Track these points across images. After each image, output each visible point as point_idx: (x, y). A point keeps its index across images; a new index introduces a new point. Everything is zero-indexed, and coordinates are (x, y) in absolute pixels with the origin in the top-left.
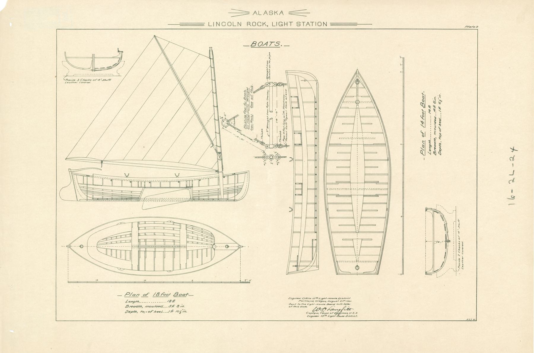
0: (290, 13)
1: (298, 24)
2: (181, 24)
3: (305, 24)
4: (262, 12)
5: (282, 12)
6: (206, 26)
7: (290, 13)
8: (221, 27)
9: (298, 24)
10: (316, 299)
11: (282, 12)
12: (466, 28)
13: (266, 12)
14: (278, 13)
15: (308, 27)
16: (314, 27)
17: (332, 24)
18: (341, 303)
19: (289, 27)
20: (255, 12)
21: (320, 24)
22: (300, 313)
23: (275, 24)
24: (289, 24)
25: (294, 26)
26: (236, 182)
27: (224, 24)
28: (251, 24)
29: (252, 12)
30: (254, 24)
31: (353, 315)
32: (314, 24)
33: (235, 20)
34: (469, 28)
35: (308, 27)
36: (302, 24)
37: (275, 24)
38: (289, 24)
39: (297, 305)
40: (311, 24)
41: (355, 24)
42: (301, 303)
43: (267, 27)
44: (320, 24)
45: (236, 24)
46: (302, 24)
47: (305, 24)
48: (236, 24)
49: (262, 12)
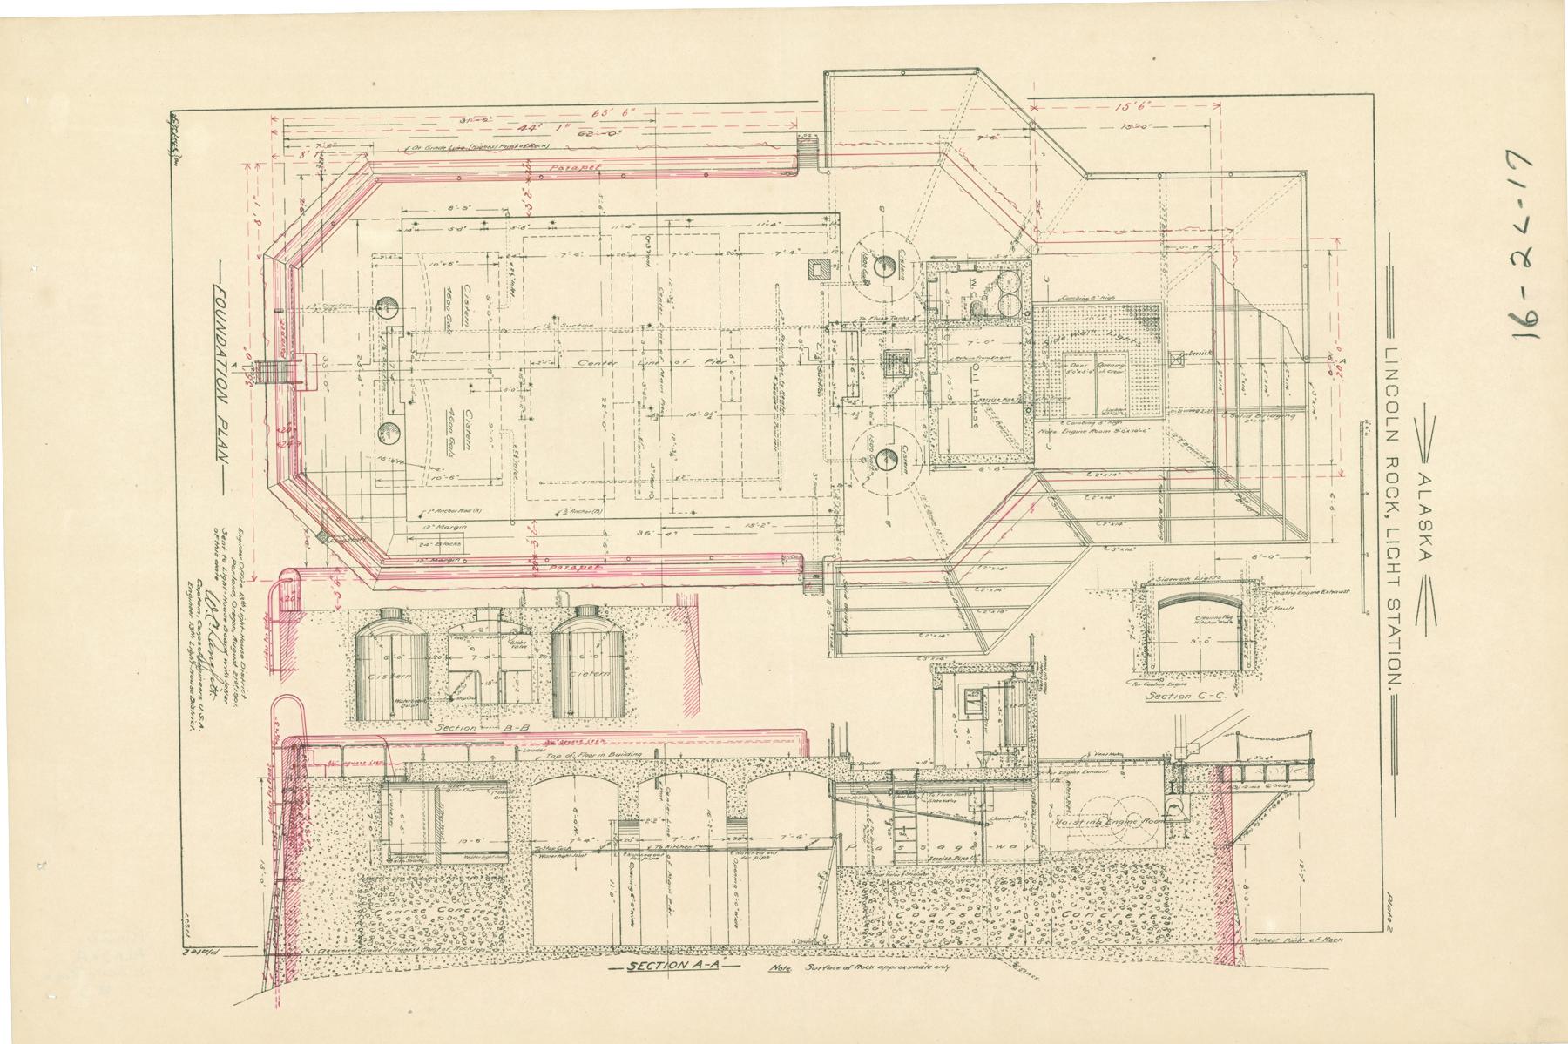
0: (1426, 582)
1: (1395, 604)
2: (1390, 270)
3: (1395, 623)
4: (1426, 469)
5: (1427, 555)
6: (1384, 341)
7: (1426, 582)
8: (1383, 383)
9: (1395, 604)
10: (239, 602)
11: (1427, 555)
12: (1387, 897)
13: (1426, 510)
14: (1426, 547)
15: (1386, 631)
16: (1386, 648)
17: (1394, 699)
18: (231, 674)
19: (1385, 578)
20: (1426, 480)
21: (1394, 664)
22: (199, 567)
23: (1394, 536)
24: (1394, 577)
25: (1388, 592)
26: (653, 238)
27: (1392, 493)
28: (1392, 469)
29: (1426, 469)
30: (1392, 407)
31: (197, 717)
32: (1395, 648)
33: (1404, 425)
34: (1387, 901)
35: (1386, 631)
36: (1395, 613)
37: (1394, 536)
38: (1394, 577)
39: (221, 551)
40: (1395, 638)
41: (1395, 772)
42: (229, 562)
43: (1383, 512)
44: (1392, 493)
45: (1393, 425)
46: (1395, 613)
47: (1395, 623)
48: (1393, 425)
49: (1426, 500)
